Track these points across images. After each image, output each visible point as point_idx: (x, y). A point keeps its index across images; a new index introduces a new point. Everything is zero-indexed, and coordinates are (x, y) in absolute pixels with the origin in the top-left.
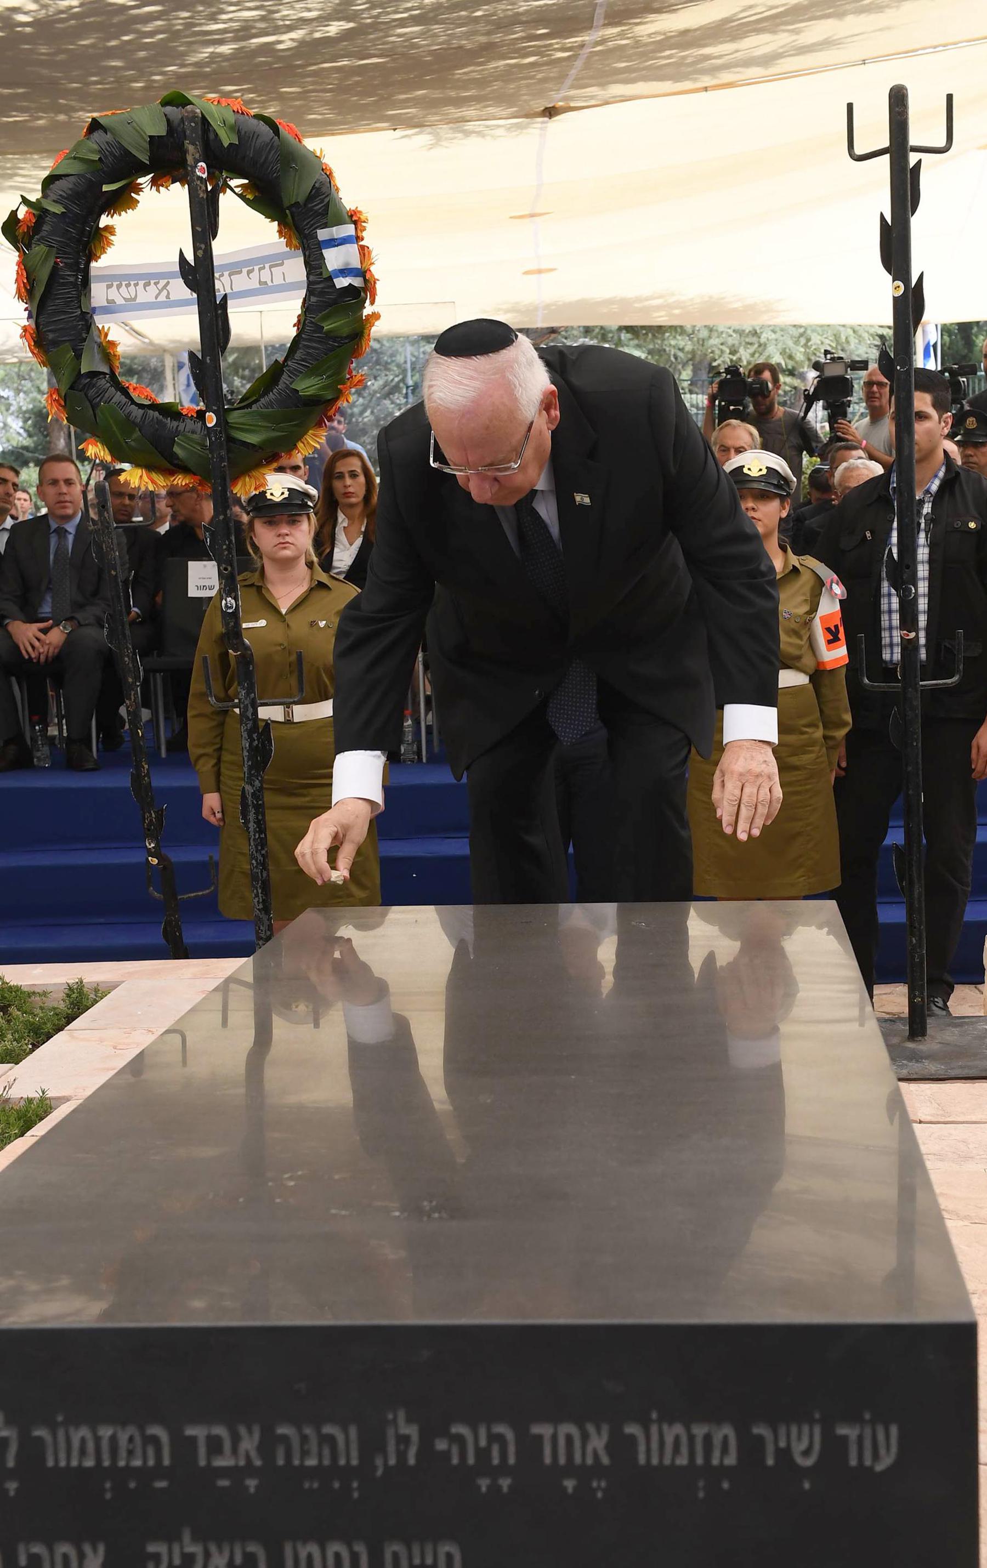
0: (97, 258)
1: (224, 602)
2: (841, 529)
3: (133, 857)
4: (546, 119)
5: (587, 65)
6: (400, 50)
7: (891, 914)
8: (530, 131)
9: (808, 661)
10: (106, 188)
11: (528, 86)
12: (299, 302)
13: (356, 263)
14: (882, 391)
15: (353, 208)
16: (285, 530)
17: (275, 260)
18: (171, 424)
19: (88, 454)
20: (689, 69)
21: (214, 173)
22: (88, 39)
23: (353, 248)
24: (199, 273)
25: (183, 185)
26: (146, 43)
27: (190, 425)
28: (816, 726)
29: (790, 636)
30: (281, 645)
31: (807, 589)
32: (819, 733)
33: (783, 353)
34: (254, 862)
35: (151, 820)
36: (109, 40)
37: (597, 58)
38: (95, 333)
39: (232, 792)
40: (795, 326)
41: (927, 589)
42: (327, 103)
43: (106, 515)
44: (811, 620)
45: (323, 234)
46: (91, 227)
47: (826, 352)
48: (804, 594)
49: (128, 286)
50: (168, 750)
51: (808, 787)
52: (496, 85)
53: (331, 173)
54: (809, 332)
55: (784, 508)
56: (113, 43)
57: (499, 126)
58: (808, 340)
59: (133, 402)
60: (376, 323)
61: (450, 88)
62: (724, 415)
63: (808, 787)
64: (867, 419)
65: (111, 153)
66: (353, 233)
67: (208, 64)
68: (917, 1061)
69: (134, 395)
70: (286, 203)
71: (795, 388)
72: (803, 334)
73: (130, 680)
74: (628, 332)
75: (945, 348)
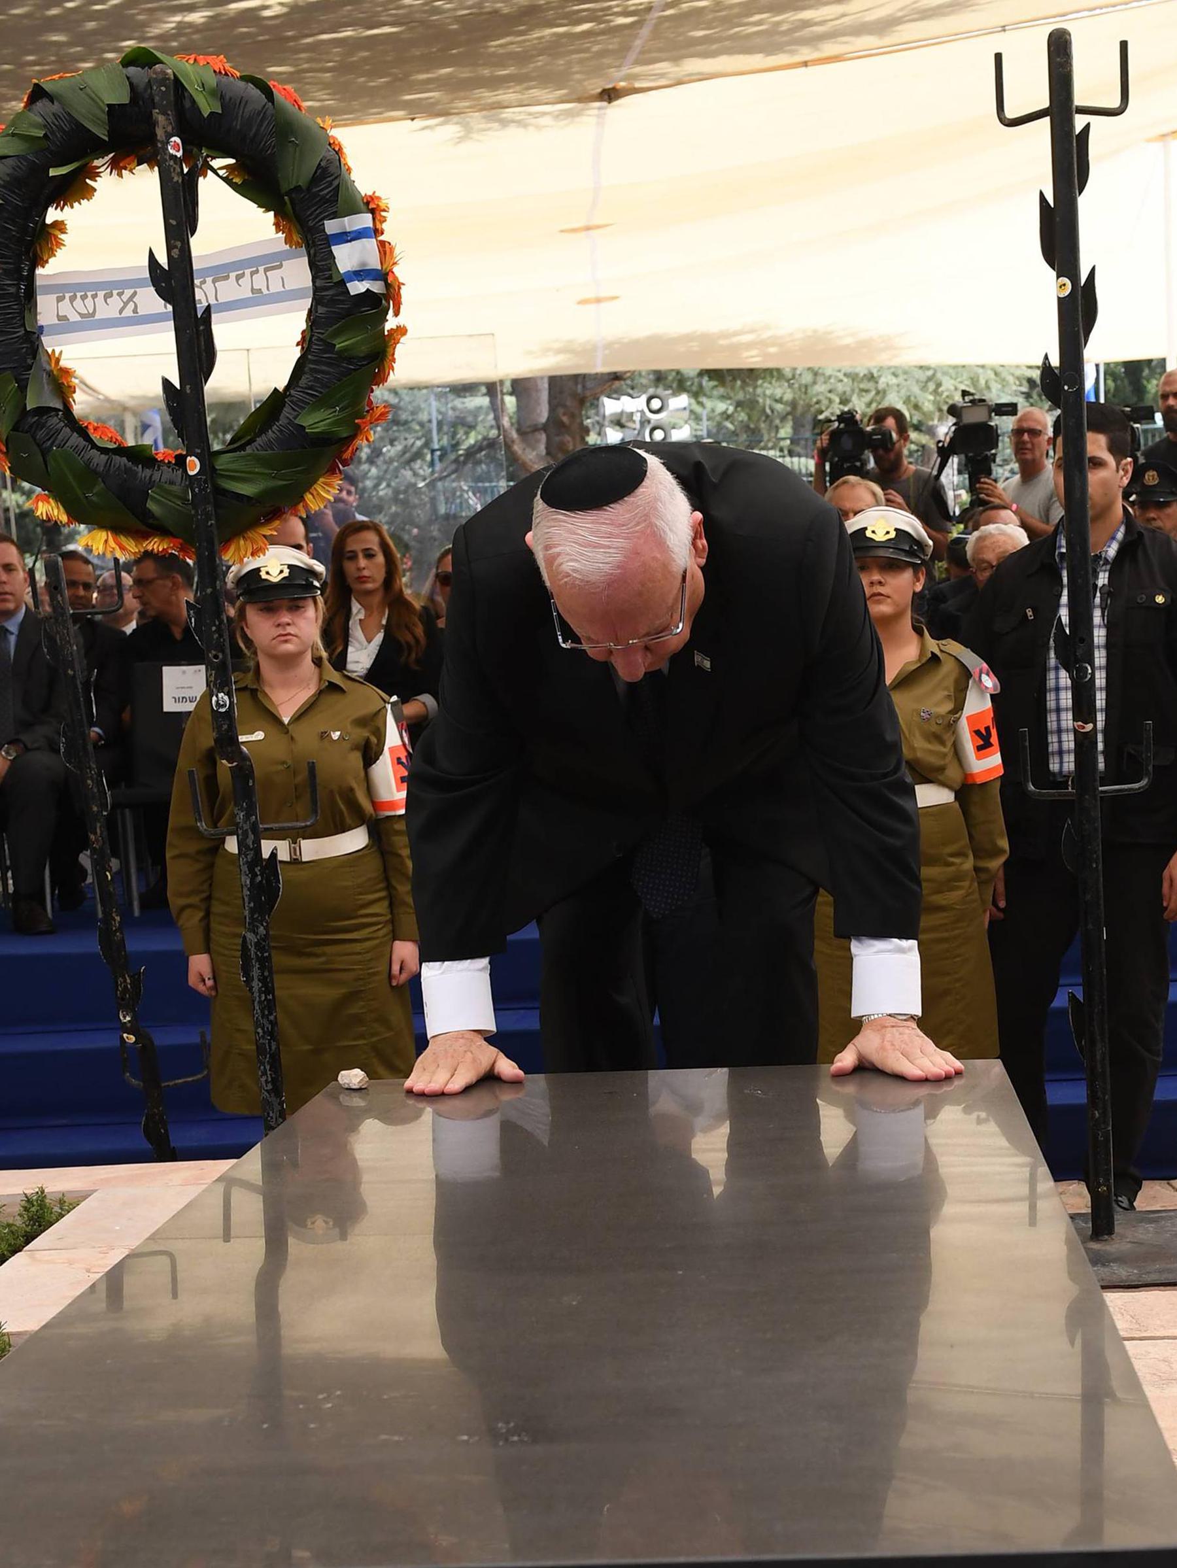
0: (44, 263)
1: (214, 698)
2: (991, 610)
3: (103, 1041)
4: (605, 104)
5: (656, 33)
6: (417, 15)
7: (1065, 1094)
8: (584, 119)
9: (953, 773)
10: (53, 172)
11: (581, 62)
12: (304, 314)
13: (374, 263)
14: (1036, 440)
15: (370, 193)
16: (286, 618)
17: (271, 262)
18: (143, 473)
19: (38, 513)
20: (785, 39)
21: (191, 151)
22: (23, 6)
23: (371, 244)
24: (174, 279)
25: (152, 168)
26: (97, 11)
27: (167, 474)
28: (965, 855)
29: (930, 742)
30: (284, 763)
31: (950, 682)
32: (969, 864)
33: (907, 401)
34: (260, 1030)
35: (126, 987)
36: (49, 8)
37: (667, 24)
38: (44, 358)
39: (226, 952)
40: (921, 367)
41: (1104, 681)
42: (326, 86)
43: (60, 599)
44: (956, 721)
45: (331, 226)
46: (36, 223)
47: (965, 393)
48: (946, 688)
49: (84, 298)
50: (143, 907)
51: (957, 932)
52: (541, 61)
53: (340, 149)
54: (939, 375)
55: (918, 580)
56: (54, 12)
57: (544, 114)
58: (939, 385)
59: (94, 446)
60: (403, 340)
61: (484, 65)
62: (836, 474)
63: (957, 932)
64: (1018, 477)
65: (60, 128)
66: (371, 225)
67: (174, 37)
68: (1103, 1265)
69: (95, 437)
70: (285, 187)
71: (923, 447)
72: (931, 378)
73: (95, 809)
74: (711, 379)
75: (1109, 396)
